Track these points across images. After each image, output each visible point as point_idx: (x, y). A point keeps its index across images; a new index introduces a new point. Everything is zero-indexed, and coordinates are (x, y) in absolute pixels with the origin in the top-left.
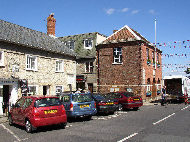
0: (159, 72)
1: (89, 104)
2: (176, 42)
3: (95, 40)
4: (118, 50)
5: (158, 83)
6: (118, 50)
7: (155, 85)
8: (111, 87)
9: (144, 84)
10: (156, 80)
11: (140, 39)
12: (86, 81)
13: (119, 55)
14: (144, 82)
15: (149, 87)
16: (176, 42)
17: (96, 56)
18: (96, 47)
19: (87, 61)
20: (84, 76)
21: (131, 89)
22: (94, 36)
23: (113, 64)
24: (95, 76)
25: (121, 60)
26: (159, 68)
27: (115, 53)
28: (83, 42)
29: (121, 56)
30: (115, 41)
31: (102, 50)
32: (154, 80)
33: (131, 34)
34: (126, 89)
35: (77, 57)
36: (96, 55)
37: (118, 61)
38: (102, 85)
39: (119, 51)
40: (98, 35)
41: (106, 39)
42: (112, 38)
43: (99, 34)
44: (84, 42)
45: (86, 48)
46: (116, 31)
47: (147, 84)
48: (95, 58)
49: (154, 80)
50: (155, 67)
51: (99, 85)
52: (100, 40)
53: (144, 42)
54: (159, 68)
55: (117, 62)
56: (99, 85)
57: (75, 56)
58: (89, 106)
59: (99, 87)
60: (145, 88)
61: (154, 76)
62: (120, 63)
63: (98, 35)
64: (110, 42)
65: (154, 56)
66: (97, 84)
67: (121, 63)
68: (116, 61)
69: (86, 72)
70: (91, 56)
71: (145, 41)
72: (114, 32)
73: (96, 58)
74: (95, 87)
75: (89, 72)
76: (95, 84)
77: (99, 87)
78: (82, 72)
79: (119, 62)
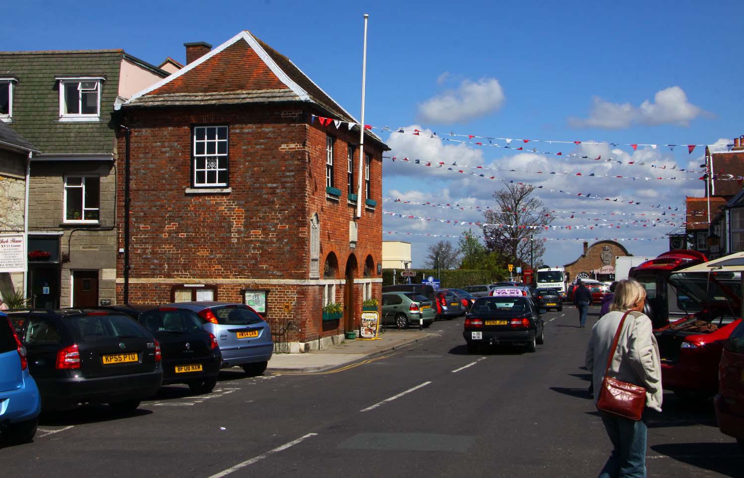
0: (373, 231)
1: (259, 329)
2: (560, 154)
3: (111, 82)
4: (211, 137)
5: (366, 275)
6: (211, 137)
7: (356, 281)
8: (181, 287)
9: (315, 276)
10: (361, 261)
11: (302, 95)
12: (66, 259)
13: (206, 155)
14: (315, 269)
15: (370, 286)
16: (560, 154)
17: (114, 154)
18: (115, 115)
19: (81, 172)
20: (57, 238)
21: (262, 297)
22: (107, 64)
23: (188, 191)
24: (111, 239)
25: (223, 177)
26: (372, 211)
27: (200, 149)
28: (56, 88)
29: (223, 162)
30: (199, 98)
31: (142, 135)
32: (352, 261)
33: (268, 71)
34: (243, 293)
35: (34, 154)
36: (116, 151)
37: (212, 179)
38: (138, 276)
39: (217, 140)
40: (125, 66)
41: (160, 83)
42: (186, 83)
43: (132, 60)
44: (62, 87)
45: (65, 117)
46: (207, 48)
47: (327, 274)
48: (110, 164)
49: (352, 261)
50: (355, 207)
51: (127, 281)
52: (135, 86)
53: (317, 113)
54: (372, 211)
55: (206, 184)
56: (127, 281)
57: (28, 152)
58: (259, 335)
59: (127, 284)
60: (317, 291)
61: (353, 246)
62: (218, 191)
63: (125, 66)
64: (179, 99)
65: (354, 165)
66: (118, 276)
67: (226, 191)
68: (201, 179)
69: (66, 221)
70: (90, 154)
71: (327, 108)
72: (195, 50)
73: (116, 164)
74: (110, 283)
75: (83, 221)
76: (109, 275)
77: (127, 284)
78: (49, 222)
79: (217, 184)
